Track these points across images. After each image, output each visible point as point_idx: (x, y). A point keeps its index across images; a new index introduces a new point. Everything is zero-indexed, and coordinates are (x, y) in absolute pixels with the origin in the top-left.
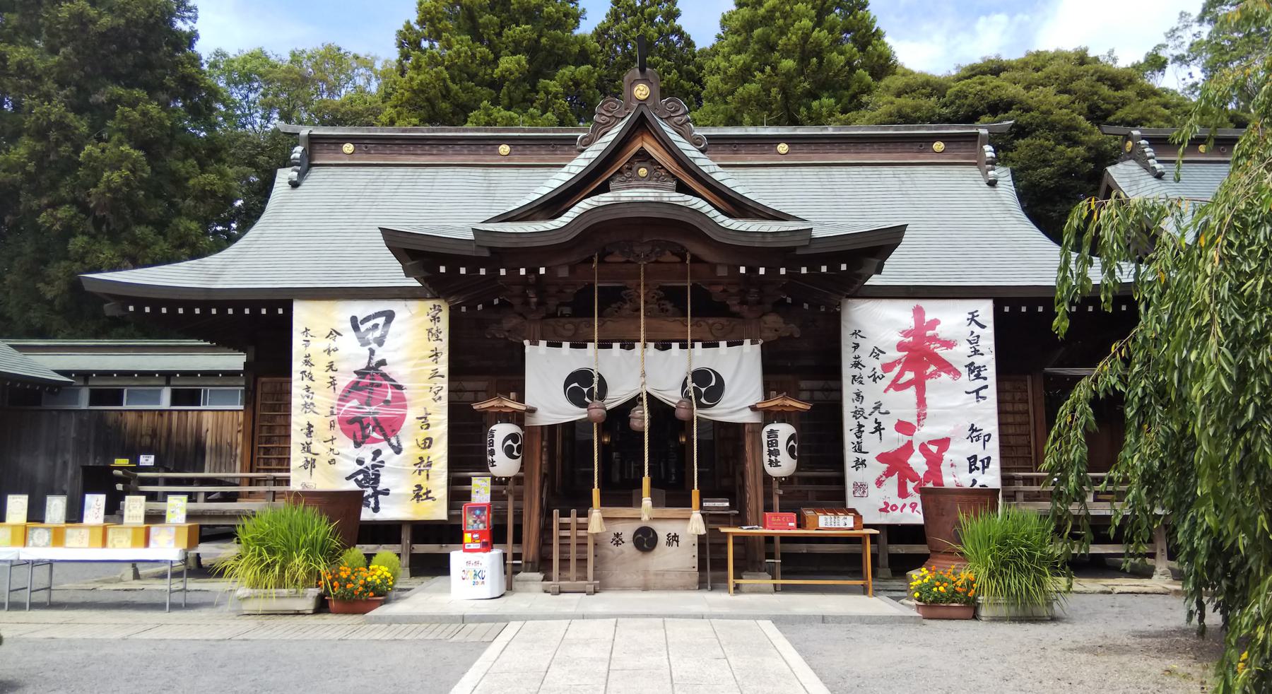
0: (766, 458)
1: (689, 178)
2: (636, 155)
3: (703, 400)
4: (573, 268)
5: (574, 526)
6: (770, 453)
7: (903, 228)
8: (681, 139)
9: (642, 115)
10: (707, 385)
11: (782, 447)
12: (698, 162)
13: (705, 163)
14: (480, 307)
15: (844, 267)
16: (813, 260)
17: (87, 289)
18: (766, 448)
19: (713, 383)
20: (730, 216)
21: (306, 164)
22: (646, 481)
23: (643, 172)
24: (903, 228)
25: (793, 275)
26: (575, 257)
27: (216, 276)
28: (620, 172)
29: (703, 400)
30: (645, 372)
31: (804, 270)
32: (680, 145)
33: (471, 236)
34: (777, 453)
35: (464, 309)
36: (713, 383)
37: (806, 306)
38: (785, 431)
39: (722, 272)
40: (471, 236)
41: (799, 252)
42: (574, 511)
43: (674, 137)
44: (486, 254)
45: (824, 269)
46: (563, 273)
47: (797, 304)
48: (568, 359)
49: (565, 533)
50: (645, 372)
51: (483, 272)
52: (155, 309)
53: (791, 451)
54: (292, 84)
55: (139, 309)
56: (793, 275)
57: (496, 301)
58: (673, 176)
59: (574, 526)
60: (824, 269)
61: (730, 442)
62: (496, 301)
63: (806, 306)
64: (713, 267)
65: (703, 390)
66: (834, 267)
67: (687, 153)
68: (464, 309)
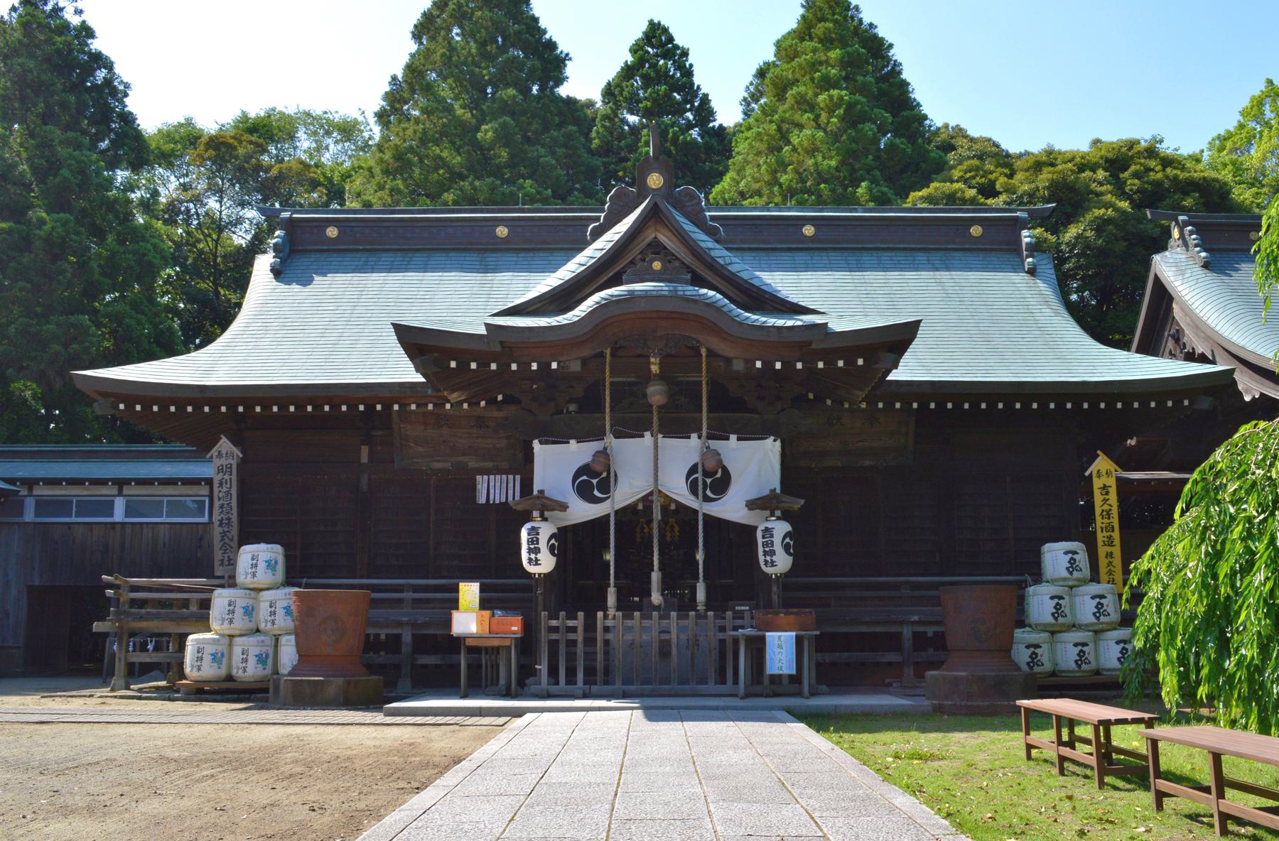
0: (761, 559)
1: (703, 271)
2: (649, 245)
3: (708, 492)
4: (585, 362)
5: (562, 630)
6: (765, 553)
7: (918, 323)
8: (696, 230)
9: (656, 204)
10: (714, 479)
11: (778, 547)
12: (713, 253)
13: (720, 253)
14: (483, 403)
15: (860, 362)
16: (829, 355)
17: (79, 386)
18: (760, 550)
19: (585, 477)
20: (747, 309)
21: (287, 250)
22: (655, 576)
23: (657, 265)
24: (918, 323)
25: (810, 370)
26: (587, 352)
27: (209, 372)
28: (632, 262)
29: (708, 492)
30: (654, 467)
31: (821, 365)
32: (686, 227)
33: (483, 331)
34: (773, 553)
35: (465, 406)
36: (585, 477)
37: (829, 402)
38: (781, 528)
39: (738, 366)
40: (483, 331)
41: (814, 346)
42: (562, 614)
43: (688, 227)
44: (498, 348)
45: (841, 363)
46: (576, 367)
47: (819, 399)
48: (577, 453)
49: (554, 636)
50: (654, 467)
51: (494, 366)
52: (164, 408)
53: (786, 548)
54: (245, 155)
55: (130, 407)
56: (810, 370)
57: (500, 398)
58: (688, 267)
59: (562, 630)
60: (841, 363)
61: (734, 542)
62: (500, 398)
63: (829, 402)
64: (728, 361)
65: (595, 481)
66: (850, 362)
67: (702, 244)
68: (465, 406)
